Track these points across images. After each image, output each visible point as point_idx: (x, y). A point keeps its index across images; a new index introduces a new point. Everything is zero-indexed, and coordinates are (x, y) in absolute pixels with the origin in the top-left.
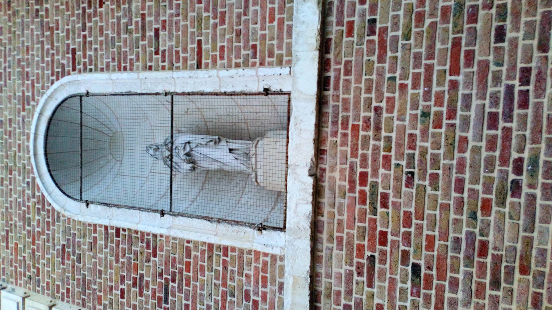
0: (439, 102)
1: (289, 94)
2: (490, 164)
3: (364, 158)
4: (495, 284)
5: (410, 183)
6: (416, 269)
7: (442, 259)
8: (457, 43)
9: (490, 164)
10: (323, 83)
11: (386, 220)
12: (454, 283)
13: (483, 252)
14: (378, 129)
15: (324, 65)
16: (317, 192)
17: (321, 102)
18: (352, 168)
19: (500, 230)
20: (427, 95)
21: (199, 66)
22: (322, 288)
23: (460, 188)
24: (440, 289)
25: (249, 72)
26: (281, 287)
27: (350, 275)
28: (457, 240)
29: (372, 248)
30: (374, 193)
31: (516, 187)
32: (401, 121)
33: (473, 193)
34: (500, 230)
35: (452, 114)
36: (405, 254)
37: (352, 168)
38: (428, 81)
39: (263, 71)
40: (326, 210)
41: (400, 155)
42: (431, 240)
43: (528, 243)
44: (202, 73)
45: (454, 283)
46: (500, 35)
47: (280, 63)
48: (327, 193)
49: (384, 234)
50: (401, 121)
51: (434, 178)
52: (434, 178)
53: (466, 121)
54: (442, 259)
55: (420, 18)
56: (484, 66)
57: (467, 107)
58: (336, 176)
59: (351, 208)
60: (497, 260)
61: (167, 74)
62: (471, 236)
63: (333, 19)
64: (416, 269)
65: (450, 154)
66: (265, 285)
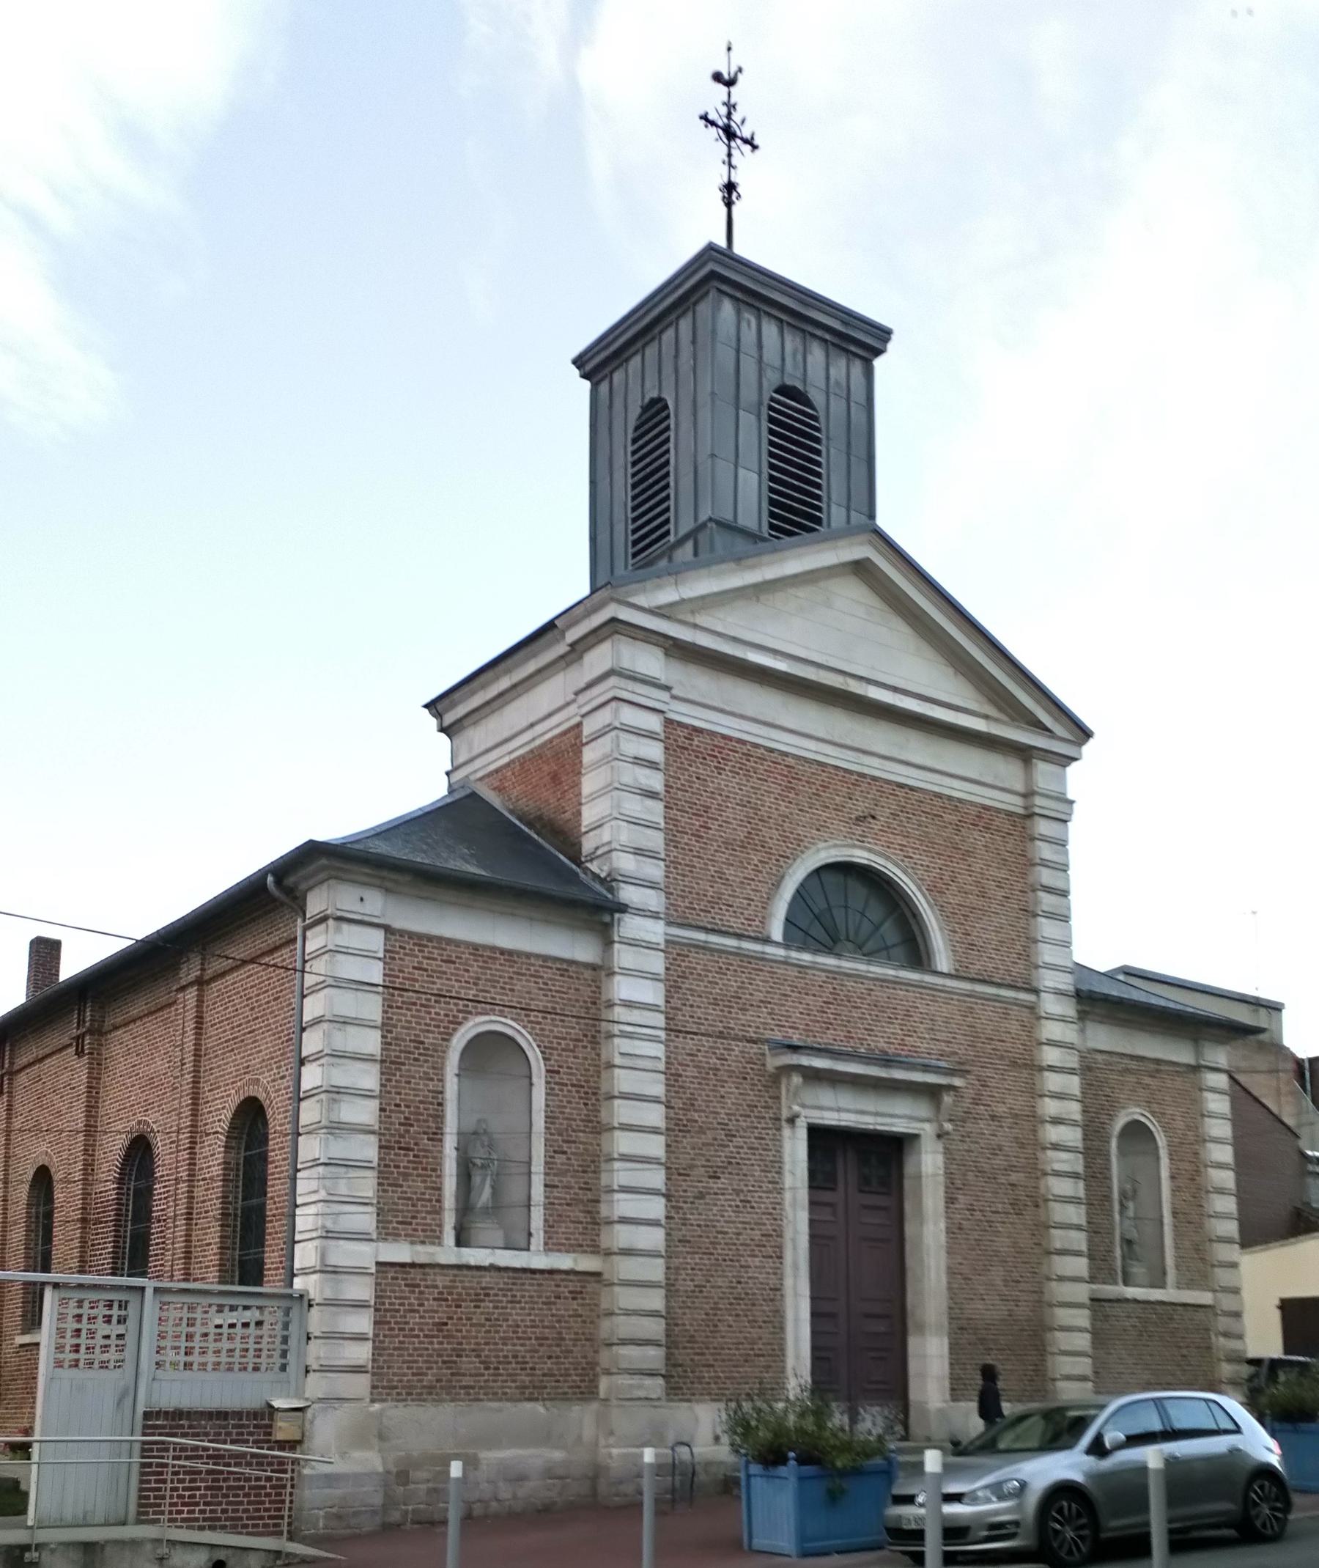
0: (524, 1332)
1: (528, 1249)
2: (497, 1357)
3: (496, 1295)
4: (444, 1362)
5: (487, 1320)
6: (446, 1324)
7: (453, 1337)
8: (547, 1339)
9: (497, 1357)
10: (533, 1271)
11: (468, 1306)
12: (441, 1343)
13: (458, 1356)
14: (399, 1349)
15: (542, 1272)
16: (479, 1268)
17: (524, 1270)
18: (492, 1288)
19: (470, 1363)
20: (526, 1326)
21: (546, 1186)
22: (427, 1270)
23: (486, 1344)
24: (437, 1337)
25: (541, 1223)
26: (423, 1243)
27: (436, 1287)
28: (461, 1344)
29: (453, 1300)
30: (399, 1349)
31: (487, 1368)
32: (515, 1315)
33: (483, 1350)
34: (470, 1363)
35: (519, 1338)
36: (451, 1318)
37: (492, 1288)
38: (532, 1327)
39: (542, 1233)
40: (469, 1273)
41: (500, 1314)
42: (461, 1331)
43: (464, 1375)
44: (542, 1188)
45: (441, 1343)
46: (550, 1357)
47: (546, 1244)
48: (479, 1273)
49: (460, 1306)
50: (515, 1315)
51: (489, 1332)
52: (489, 1332)
53: (515, 1345)
54: (453, 1337)
55: (559, 1321)
56: (537, 1351)
57: (522, 1345)
58: (487, 1279)
59: (472, 1288)
60: (455, 1362)
61: (542, 1159)
62: (464, 1350)
63: (564, 1276)
64: (446, 1324)
65: (501, 1338)
66: (423, 1231)
